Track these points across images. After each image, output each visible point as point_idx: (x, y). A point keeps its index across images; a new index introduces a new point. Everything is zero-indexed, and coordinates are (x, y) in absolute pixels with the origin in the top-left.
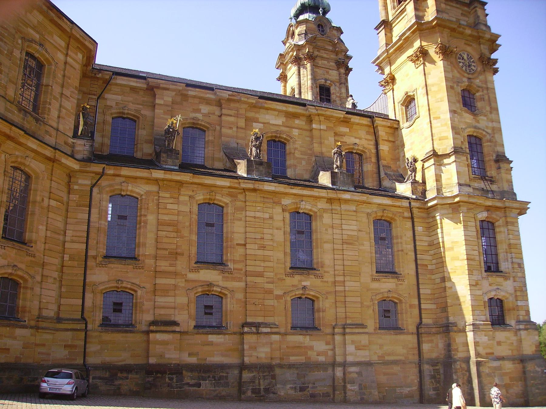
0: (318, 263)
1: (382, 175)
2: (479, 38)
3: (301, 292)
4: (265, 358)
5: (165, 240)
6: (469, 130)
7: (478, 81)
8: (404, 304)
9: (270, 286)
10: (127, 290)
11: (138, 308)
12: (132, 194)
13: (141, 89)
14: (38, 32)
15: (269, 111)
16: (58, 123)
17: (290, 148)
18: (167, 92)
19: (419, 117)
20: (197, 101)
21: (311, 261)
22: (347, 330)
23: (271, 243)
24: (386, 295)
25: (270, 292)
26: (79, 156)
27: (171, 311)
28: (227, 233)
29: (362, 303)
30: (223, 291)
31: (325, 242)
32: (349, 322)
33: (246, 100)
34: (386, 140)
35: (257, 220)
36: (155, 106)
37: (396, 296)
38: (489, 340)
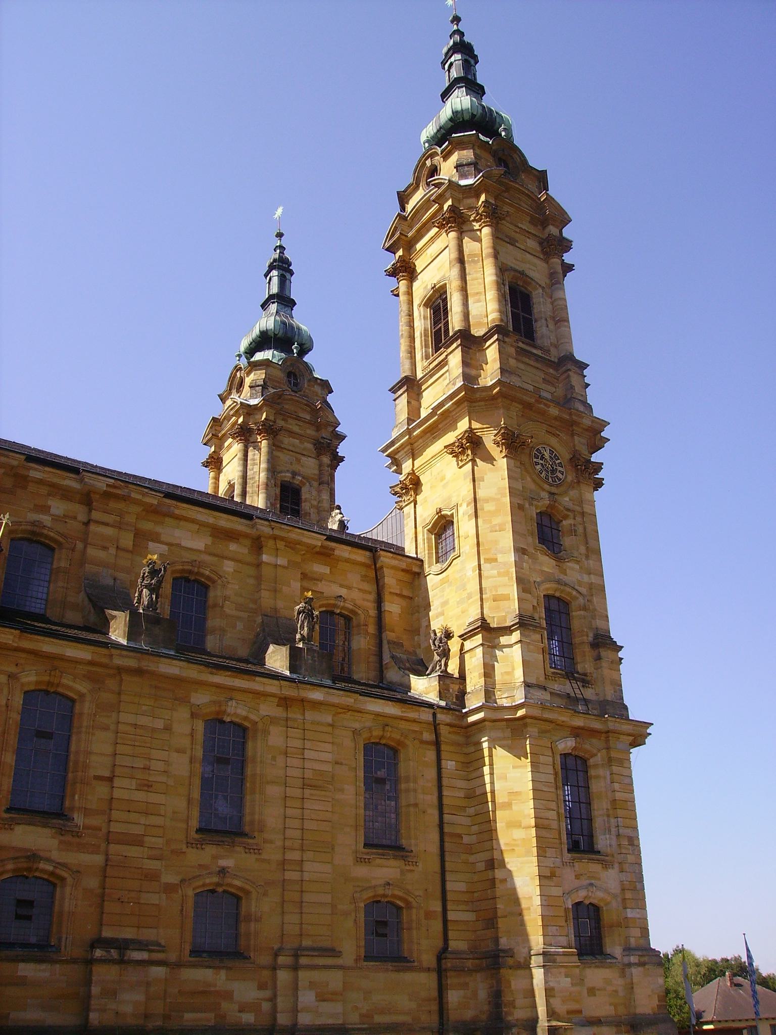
0: (252, 823)
1: (387, 658)
6: (548, 586)
7: (567, 499)
8: (414, 911)
15: (182, 523)
19: (459, 556)
20: (44, 490)
21: (241, 819)
23: (163, 779)
25: (153, 877)
31: (268, 783)
32: (306, 943)
33: (139, 497)
37: (400, 894)
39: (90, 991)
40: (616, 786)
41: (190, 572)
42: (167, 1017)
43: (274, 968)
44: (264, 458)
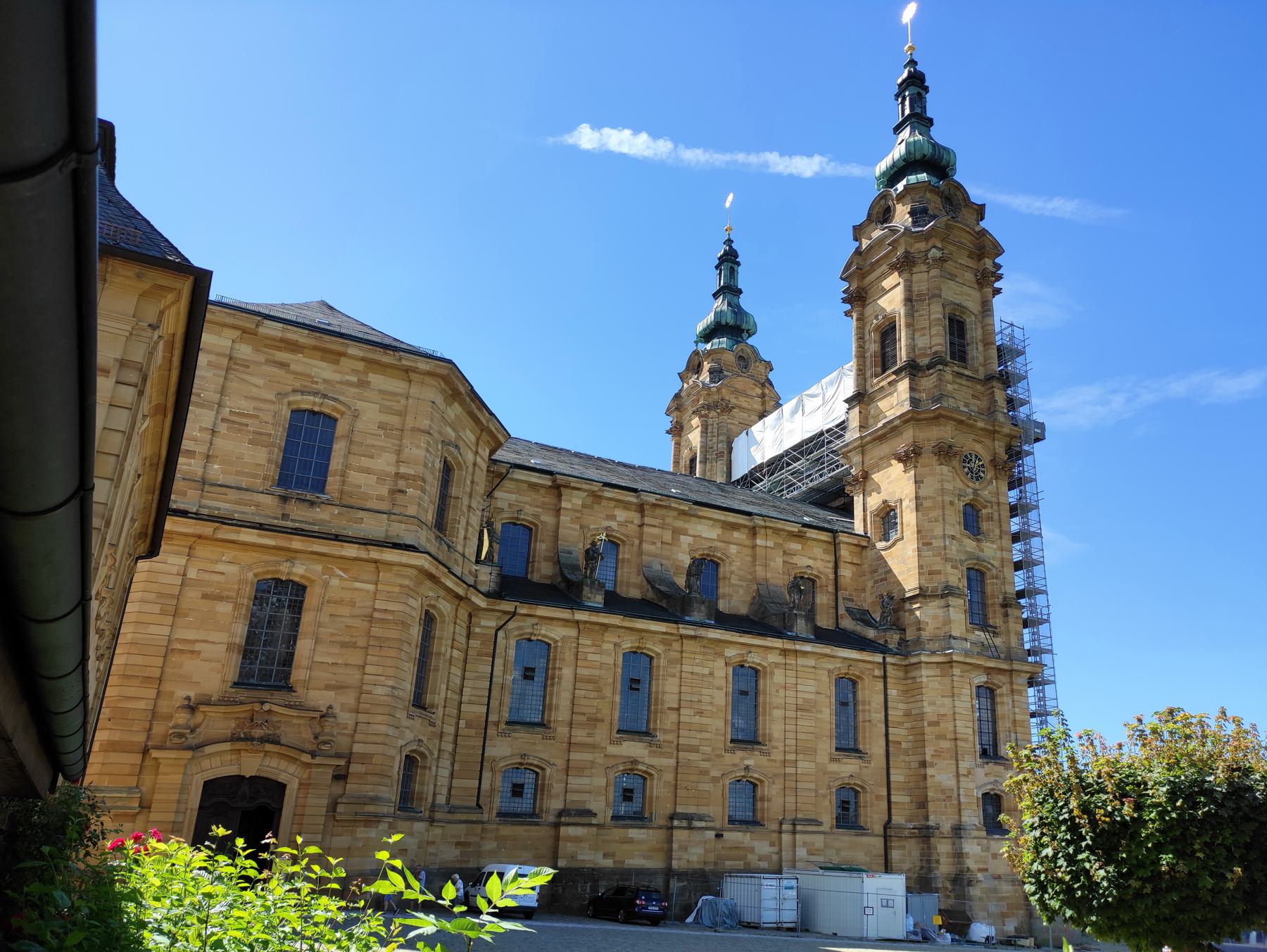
0: (764, 735)
1: (842, 611)
2: (994, 432)
3: (743, 774)
4: (697, 862)
5: (583, 702)
6: (970, 562)
7: (986, 493)
8: (869, 795)
9: (706, 765)
10: (532, 768)
11: (546, 792)
12: (543, 639)
13: (543, 486)
14: (454, 430)
15: (702, 520)
16: (465, 546)
17: (725, 572)
18: (577, 492)
19: (902, 538)
20: (612, 504)
21: (756, 731)
22: (799, 828)
23: (709, 708)
24: (847, 782)
25: (705, 772)
26: (484, 588)
27: (585, 797)
28: (657, 692)
29: (816, 791)
30: (649, 771)
31: (774, 708)
32: (800, 816)
33: (676, 506)
34: (850, 563)
35: (695, 677)
36: (560, 509)
37: (859, 783)
38: (982, 851)
39: (672, 847)
40: (1017, 710)
41: (708, 555)
42: (716, 864)
43: (780, 832)
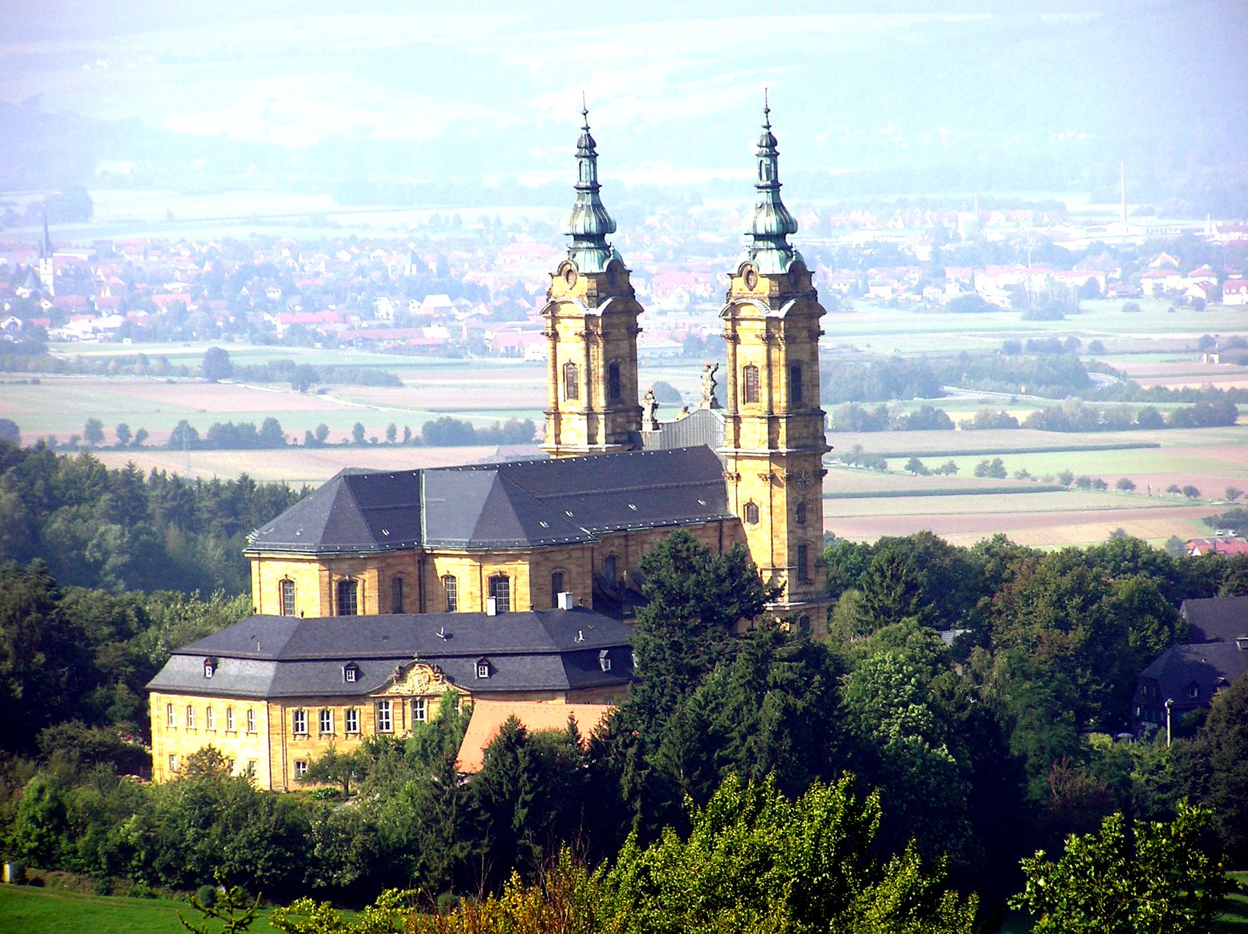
44: (601, 350)
